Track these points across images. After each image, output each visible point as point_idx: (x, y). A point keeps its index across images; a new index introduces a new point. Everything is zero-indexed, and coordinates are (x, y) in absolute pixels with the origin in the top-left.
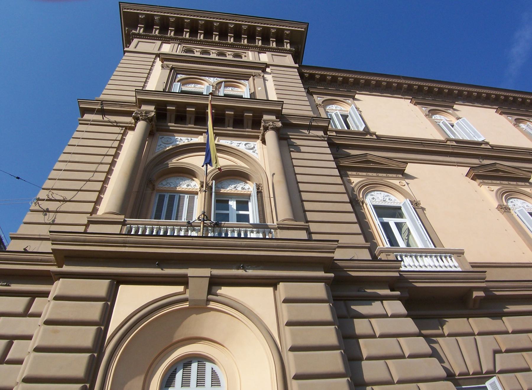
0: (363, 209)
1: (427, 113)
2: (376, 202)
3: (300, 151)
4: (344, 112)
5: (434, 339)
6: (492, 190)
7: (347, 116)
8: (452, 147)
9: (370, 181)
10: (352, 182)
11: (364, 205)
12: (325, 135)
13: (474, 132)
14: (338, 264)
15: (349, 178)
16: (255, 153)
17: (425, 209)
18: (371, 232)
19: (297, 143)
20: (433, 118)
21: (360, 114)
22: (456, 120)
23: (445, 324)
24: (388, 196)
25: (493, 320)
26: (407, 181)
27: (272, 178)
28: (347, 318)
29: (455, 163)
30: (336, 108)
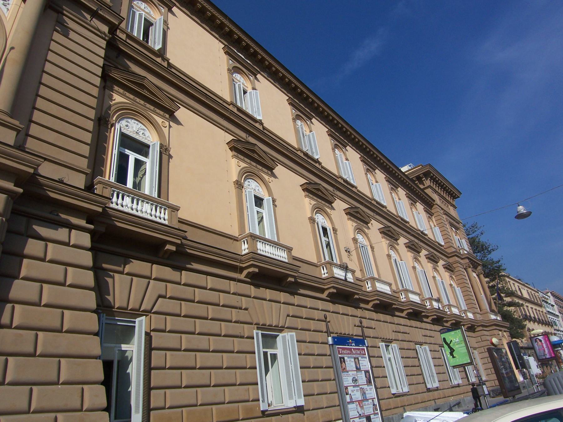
0: (109, 132)
1: (231, 68)
2: (128, 131)
3: (66, 36)
4: (151, 18)
5: (112, 274)
6: (240, 165)
7: (152, 24)
8: (230, 112)
9: (133, 107)
10: (113, 99)
11: (113, 128)
12: (108, 33)
13: (258, 108)
14: (39, 180)
15: (112, 93)
16: (6, 7)
17: (173, 157)
18: (104, 159)
19: (68, 24)
20: (234, 75)
21: (166, 30)
22: (251, 89)
23: (129, 264)
24: (144, 130)
25: (173, 270)
26: (172, 124)
27: (8, 52)
28: (22, 235)
29: (224, 127)
30: (145, 8)
